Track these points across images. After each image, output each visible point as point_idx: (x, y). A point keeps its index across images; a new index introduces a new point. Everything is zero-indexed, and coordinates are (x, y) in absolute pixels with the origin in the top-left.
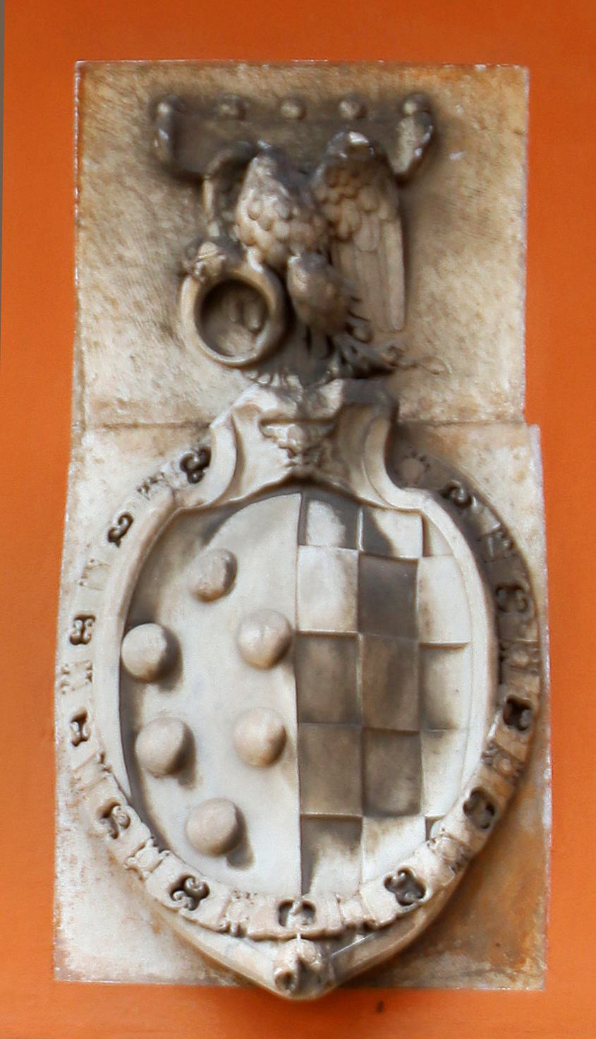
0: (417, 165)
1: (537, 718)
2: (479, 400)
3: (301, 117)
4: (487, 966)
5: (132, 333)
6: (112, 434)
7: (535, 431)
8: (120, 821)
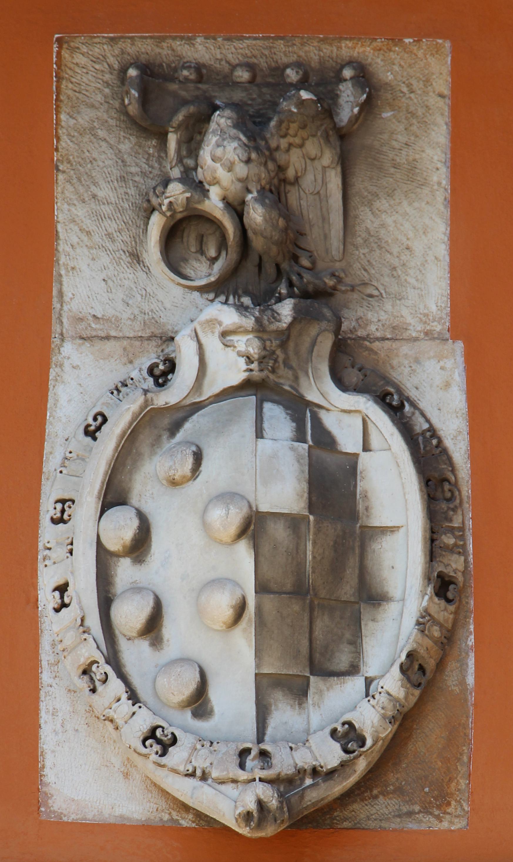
0: (354, 120)
1: (461, 591)
2: (409, 319)
3: (252, 81)
4: (417, 808)
5: (105, 259)
6: (87, 344)
7: (459, 346)
8: (98, 677)
